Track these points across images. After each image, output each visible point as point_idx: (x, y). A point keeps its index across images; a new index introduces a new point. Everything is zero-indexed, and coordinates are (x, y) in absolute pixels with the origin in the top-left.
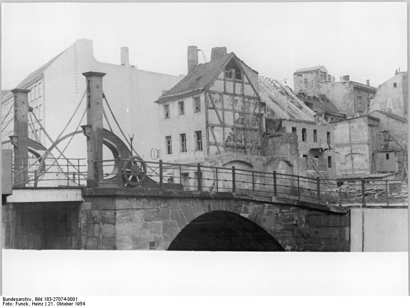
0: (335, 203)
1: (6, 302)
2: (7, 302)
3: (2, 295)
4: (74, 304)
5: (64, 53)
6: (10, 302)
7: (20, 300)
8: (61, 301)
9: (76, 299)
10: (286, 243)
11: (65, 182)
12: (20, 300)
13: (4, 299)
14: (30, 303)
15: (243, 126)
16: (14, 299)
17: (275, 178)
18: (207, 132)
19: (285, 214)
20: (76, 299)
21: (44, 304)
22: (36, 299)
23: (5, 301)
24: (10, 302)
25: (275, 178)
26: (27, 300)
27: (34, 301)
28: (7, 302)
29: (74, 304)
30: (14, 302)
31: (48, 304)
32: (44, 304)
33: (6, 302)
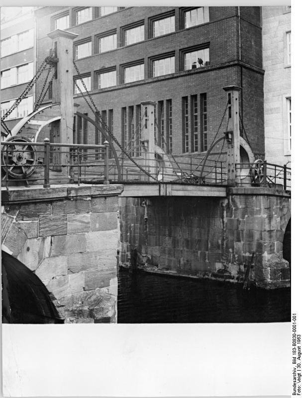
0: (206, 255)
1: (297, 392)
2: (297, 391)
3: (290, 396)
5: (4, 282)
6: (297, 389)
7: (295, 379)
8: (297, 342)
10: (35, 209)
11: (163, 193)
12: (295, 379)
13: (294, 394)
15: (151, 109)
16: (295, 384)
17: (285, 172)
18: (183, 105)
19: (179, 171)
22: (294, 363)
24: (297, 389)
25: (285, 172)
26: (295, 371)
27: (297, 372)
28: (297, 391)
31: (299, 369)
33: (297, 392)
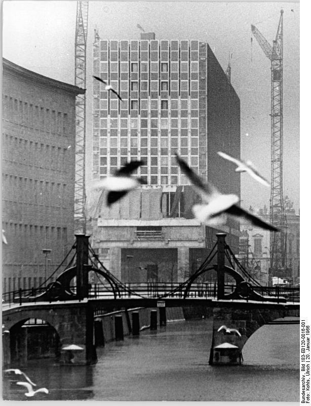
2: (306, 399)
4: (308, 336)
6: (306, 396)
9: (303, 321)
12: (304, 386)
13: (303, 402)
14: (307, 378)
16: (304, 392)
20: (303, 321)
21: (308, 363)
23: (305, 401)
24: (306, 396)
26: (304, 379)
28: (306, 399)
29: (308, 336)
30: (306, 392)
31: (308, 360)
32: (308, 363)
